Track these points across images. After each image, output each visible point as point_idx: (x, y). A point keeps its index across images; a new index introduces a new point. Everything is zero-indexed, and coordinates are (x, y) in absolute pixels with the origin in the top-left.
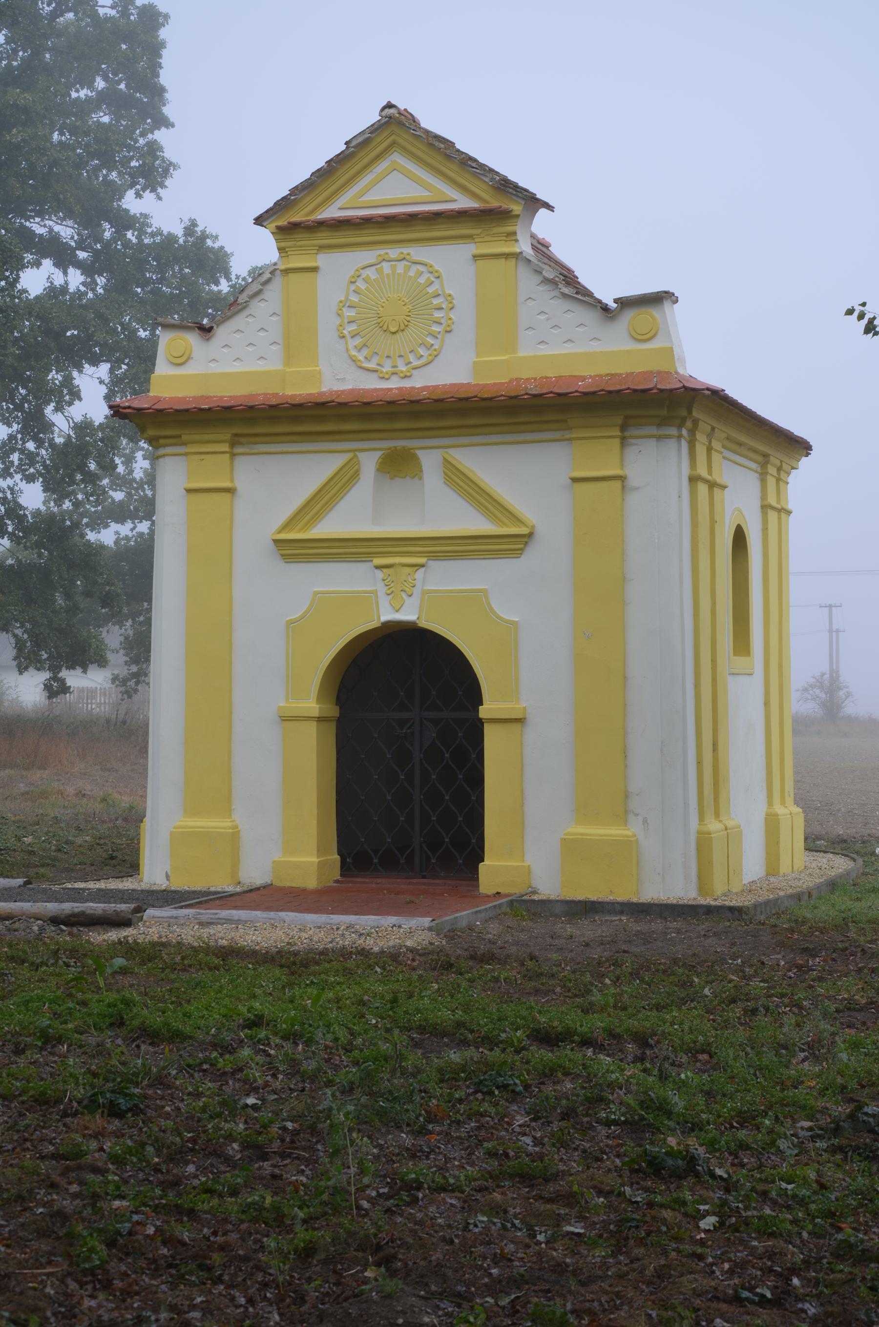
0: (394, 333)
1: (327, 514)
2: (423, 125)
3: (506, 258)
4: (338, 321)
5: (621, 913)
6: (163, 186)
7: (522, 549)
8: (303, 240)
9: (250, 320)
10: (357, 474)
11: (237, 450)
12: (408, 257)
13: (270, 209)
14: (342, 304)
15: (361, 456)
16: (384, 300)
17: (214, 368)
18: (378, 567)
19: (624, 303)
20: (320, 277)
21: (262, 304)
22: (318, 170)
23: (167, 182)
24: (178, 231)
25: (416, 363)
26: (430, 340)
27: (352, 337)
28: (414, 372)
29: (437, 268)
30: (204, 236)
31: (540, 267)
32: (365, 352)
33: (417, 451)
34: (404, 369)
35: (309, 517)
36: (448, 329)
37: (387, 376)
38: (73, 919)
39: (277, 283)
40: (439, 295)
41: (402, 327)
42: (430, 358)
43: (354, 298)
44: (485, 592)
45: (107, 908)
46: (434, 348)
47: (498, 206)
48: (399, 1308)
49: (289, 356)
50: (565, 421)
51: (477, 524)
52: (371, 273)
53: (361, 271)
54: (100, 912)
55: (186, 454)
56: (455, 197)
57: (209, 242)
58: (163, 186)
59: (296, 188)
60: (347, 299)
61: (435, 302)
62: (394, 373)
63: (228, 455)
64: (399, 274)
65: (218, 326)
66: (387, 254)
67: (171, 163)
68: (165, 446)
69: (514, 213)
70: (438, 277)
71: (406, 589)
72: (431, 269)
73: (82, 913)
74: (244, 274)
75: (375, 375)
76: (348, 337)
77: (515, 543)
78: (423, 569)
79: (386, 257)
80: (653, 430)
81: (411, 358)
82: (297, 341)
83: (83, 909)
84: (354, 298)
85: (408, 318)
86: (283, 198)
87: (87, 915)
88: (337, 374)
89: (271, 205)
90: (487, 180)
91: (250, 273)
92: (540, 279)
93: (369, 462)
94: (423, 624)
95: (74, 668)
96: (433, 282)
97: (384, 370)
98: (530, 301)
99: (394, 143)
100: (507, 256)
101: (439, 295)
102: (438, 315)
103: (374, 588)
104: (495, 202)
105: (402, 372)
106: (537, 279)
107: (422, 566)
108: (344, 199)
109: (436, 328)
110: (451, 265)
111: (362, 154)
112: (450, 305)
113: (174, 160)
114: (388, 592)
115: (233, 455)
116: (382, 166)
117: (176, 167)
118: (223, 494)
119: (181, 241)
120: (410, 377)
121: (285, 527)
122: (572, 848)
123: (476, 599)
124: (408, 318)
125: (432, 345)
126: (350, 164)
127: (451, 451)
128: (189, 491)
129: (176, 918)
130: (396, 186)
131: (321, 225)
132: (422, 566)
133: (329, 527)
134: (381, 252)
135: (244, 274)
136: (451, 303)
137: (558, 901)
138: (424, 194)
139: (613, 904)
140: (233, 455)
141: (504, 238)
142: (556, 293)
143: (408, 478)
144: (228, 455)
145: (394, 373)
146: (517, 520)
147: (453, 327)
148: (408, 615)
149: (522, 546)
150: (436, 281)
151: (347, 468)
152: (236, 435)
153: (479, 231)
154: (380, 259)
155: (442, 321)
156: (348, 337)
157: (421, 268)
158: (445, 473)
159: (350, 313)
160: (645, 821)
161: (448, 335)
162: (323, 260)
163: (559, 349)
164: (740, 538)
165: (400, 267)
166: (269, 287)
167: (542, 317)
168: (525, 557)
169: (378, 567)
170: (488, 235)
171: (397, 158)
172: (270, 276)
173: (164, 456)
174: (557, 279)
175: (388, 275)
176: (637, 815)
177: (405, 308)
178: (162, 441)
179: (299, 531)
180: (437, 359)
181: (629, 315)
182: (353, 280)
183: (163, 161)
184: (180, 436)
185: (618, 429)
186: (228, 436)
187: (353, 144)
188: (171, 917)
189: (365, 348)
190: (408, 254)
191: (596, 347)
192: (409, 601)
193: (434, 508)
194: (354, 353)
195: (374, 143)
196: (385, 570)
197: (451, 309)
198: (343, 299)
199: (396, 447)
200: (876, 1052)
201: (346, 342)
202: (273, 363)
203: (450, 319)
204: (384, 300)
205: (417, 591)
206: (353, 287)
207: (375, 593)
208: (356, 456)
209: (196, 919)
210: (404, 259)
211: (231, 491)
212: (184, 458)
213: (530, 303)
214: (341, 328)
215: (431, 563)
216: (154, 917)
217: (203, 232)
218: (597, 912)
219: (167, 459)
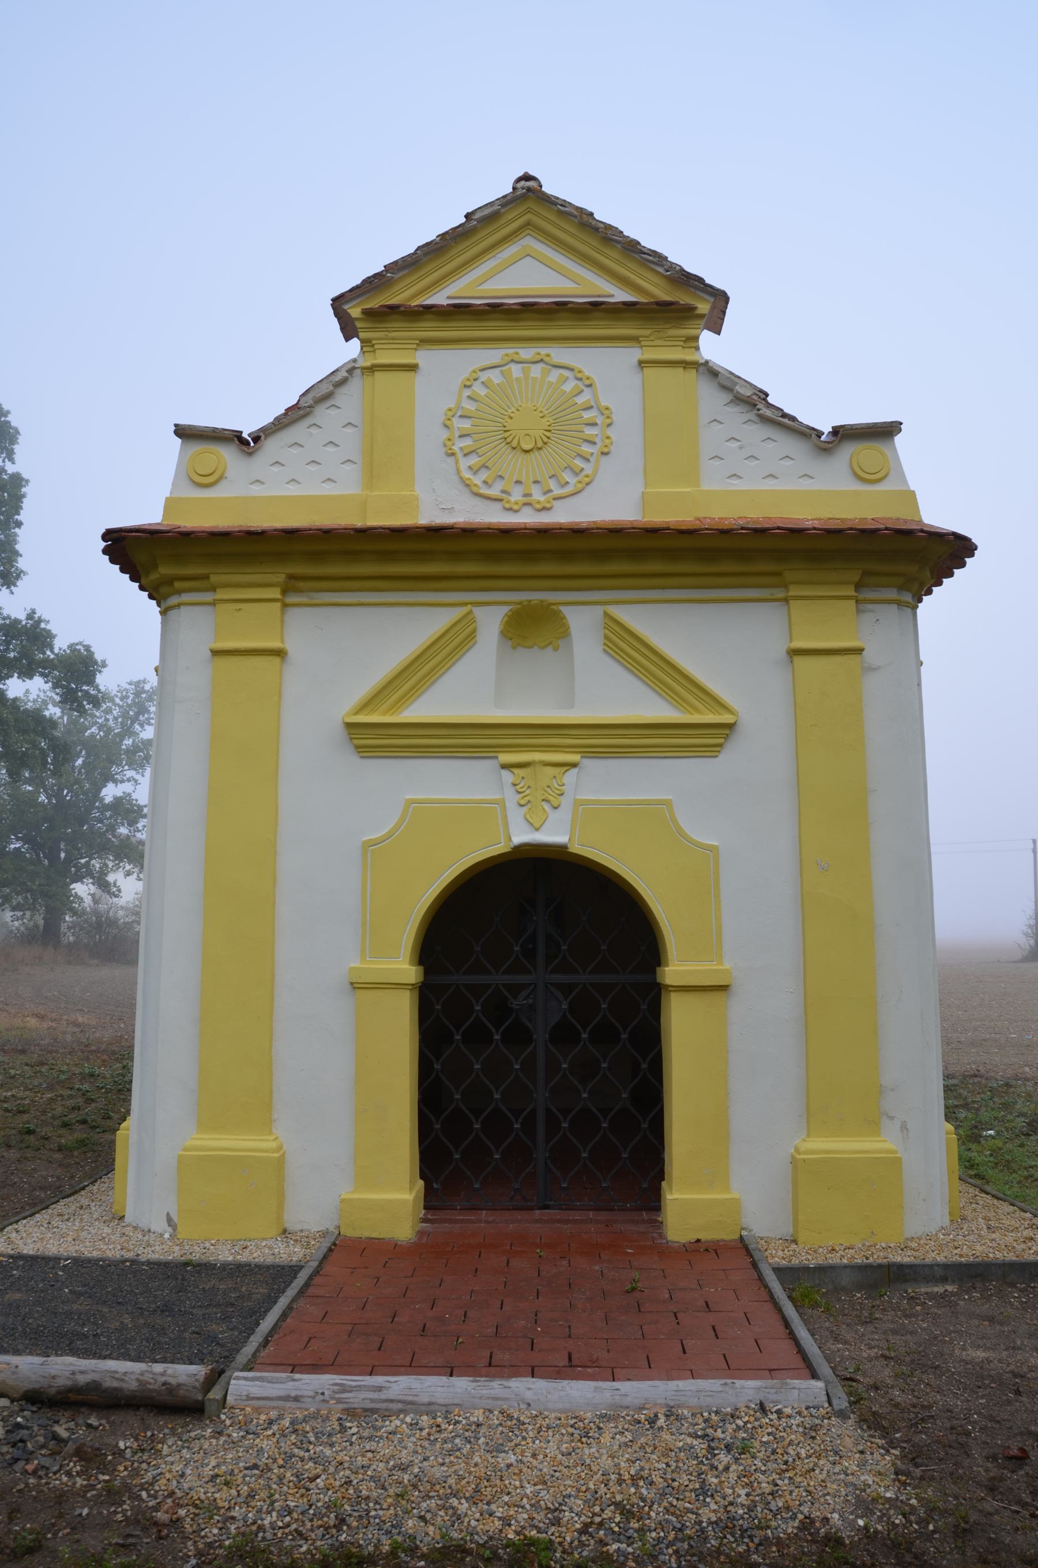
0: (526, 452)
1: (418, 697)
3: (684, 368)
4: (445, 434)
5: (944, 1280)
6: (15, 585)
7: (720, 745)
8: (398, 329)
9: (314, 430)
10: (471, 637)
11: (291, 599)
12: (546, 359)
13: (357, 287)
15: (478, 611)
16: (513, 409)
18: (504, 766)
19: (842, 434)
20: (419, 381)
21: (333, 412)
22: (428, 244)
23: (19, 583)
24: (22, 616)
25: (558, 492)
26: (579, 463)
27: (465, 455)
28: (556, 503)
29: (587, 374)
30: (40, 620)
31: (733, 381)
32: (484, 475)
33: (562, 608)
34: (542, 499)
35: (401, 692)
36: (606, 450)
37: (516, 507)
38: (72, 1397)
39: (356, 384)
40: (592, 407)
41: (540, 444)
42: (580, 486)
43: (470, 406)
44: (667, 803)
45: (147, 1377)
46: (583, 473)
47: (669, 303)
49: (371, 475)
50: (779, 574)
51: (658, 710)
52: (495, 376)
53: (480, 374)
54: (132, 1385)
55: (213, 603)
56: (612, 292)
57: (43, 625)
58: (15, 585)
59: (396, 263)
60: (459, 406)
61: (587, 415)
62: (525, 504)
63: (279, 604)
64: (535, 379)
65: (266, 437)
66: (517, 353)
67: (22, 571)
68: (179, 592)
69: (698, 312)
70: (590, 386)
71: (551, 798)
72: (579, 375)
73: (94, 1387)
74: (65, 647)
75: (498, 506)
76: (460, 455)
78: (575, 771)
79: (516, 358)
80: (892, 594)
81: (552, 484)
83: (96, 1377)
84: (470, 406)
85: (548, 434)
86: (375, 276)
87: (106, 1390)
88: (438, 499)
89: (359, 282)
90: (661, 270)
91: (68, 647)
92: (728, 397)
93: (491, 621)
94: (576, 848)
96: (582, 391)
97: (513, 499)
98: (715, 423)
99: (528, 224)
100: (686, 365)
101: (592, 407)
102: (590, 431)
103: (497, 797)
105: (539, 502)
106: (727, 397)
107: (574, 765)
109: (586, 448)
110: (609, 371)
111: (484, 233)
112: (608, 421)
113: (24, 569)
114: (522, 802)
115: (285, 606)
116: (510, 250)
117: (25, 573)
118: (270, 658)
119: (24, 623)
120: (549, 509)
121: (365, 706)
123: (658, 814)
124: (548, 434)
125: (582, 470)
126: (467, 243)
128: (216, 653)
129: (296, 1399)
131: (429, 310)
132: (574, 765)
133: (427, 708)
135: (65, 647)
136: (608, 417)
137: (846, 1267)
139: (931, 1266)
140: (285, 606)
141: (682, 343)
142: (752, 415)
143: (536, 647)
144: (279, 604)
145: (525, 504)
146: (725, 708)
147: (612, 448)
148: (554, 832)
149: (722, 740)
150: (587, 390)
151: (457, 629)
152: (291, 577)
153: (648, 332)
154: (508, 359)
155: (597, 440)
156: (460, 455)
157: (566, 373)
158: (606, 637)
160: (904, 1127)
161: (604, 458)
162: (422, 357)
163: (746, 485)
165: (536, 371)
166: (343, 389)
167: (734, 445)
168: (721, 756)
169: (504, 766)
170: (660, 338)
171: (529, 242)
172: (346, 374)
173: (179, 605)
174: (755, 397)
175: (518, 379)
176: (892, 1118)
177: (543, 420)
178: (177, 585)
179: (385, 713)
180: (589, 488)
181: (848, 451)
182: (468, 383)
183: (17, 569)
184: (206, 577)
185: (853, 587)
186: (281, 578)
187: (477, 216)
188: (286, 1398)
189: (483, 470)
190: (548, 355)
191: (806, 485)
194: (467, 475)
195: (503, 221)
196: (516, 771)
197: (609, 425)
198: (452, 406)
199: (530, 601)
201: (457, 462)
203: (608, 438)
204: (513, 409)
205: (566, 802)
206: (467, 392)
207: (501, 803)
208: (470, 612)
209: (339, 1401)
210: (542, 360)
211: (279, 653)
212: (209, 609)
213: (716, 427)
214: (449, 443)
215: (586, 762)
216: (249, 1398)
217: (40, 618)
218: (906, 1281)
219: (184, 609)
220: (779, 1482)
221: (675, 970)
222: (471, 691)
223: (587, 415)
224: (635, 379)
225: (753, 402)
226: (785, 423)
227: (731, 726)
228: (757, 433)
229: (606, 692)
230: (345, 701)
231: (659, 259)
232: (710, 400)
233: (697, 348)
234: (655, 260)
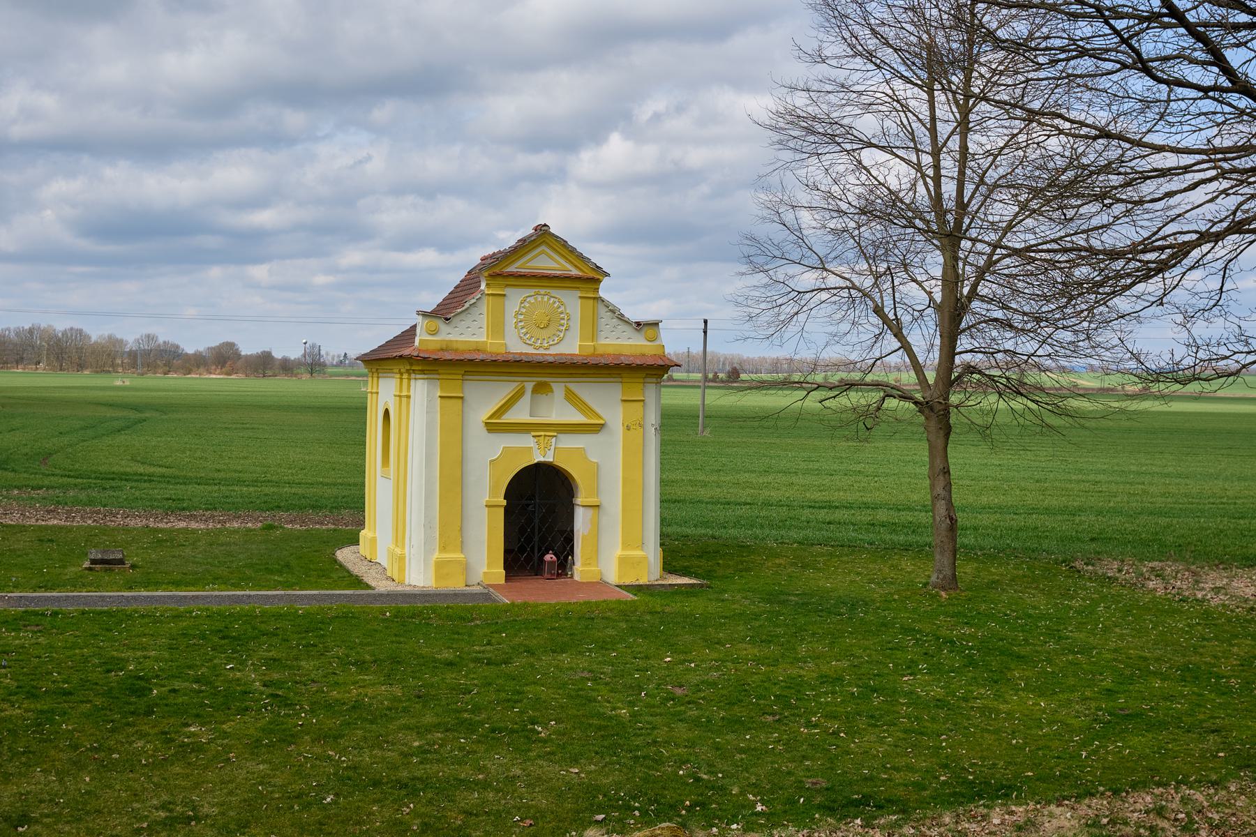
2: (190, 350)
8: (500, 281)
10: (523, 394)
14: (517, 314)
17: (451, 337)
47: (588, 279)
77: (597, 428)
82: (497, 327)
88: (515, 344)
93: (529, 386)
108: (518, 264)
110: (571, 302)
122: (623, 561)
131: (511, 275)
133: (509, 417)
146: (601, 418)
162: (507, 291)
163: (617, 342)
164: (387, 412)
165: (546, 298)
191: (630, 342)
193: (558, 410)
200: (1253, 822)
227: (603, 425)
230: (484, 414)
233: (597, 290)
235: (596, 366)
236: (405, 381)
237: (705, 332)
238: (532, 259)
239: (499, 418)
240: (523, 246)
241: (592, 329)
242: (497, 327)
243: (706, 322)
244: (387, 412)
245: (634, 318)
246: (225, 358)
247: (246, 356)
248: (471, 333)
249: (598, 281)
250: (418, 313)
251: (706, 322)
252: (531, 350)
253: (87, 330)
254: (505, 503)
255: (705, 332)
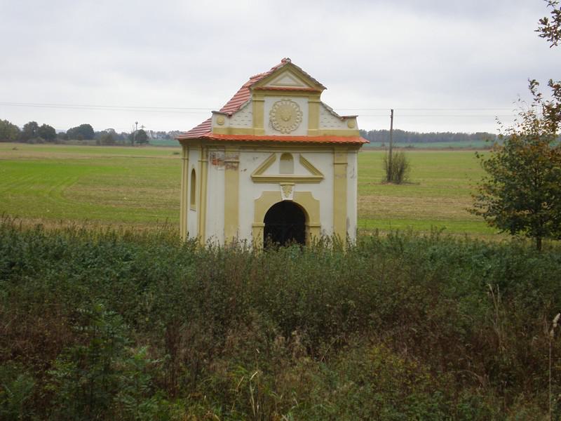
10: (275, 160)
14: (271, 111)
15: (277, 154)
19: (345, 118)
20: (265, 103)
43: (275, 110)
47: (314, 90)
48: (372, 340)
49: (255, 125)
52: (280, 104)
61: (298, 113)
77: (318, 180)
82: (257, 121)
84: (275, 110)
88: (268, 132)
93: (278, 156)
94: (294, 201)
95: (26, 126)
104: (316, 88)
108: (272, 82)
110: (302, 103)
116: (284, 74)
127: (302, 154)
130: (287, 81)
133: (267, 174)
134: (282, 98)
138: (295, 83)
146: (321, 174)
148: (290, 198)
159: (274, 114)
162: (266, 99)
163: (328, 129)
164: (193, 171)
165: (288, 103)
191: (340, 129)
192: (290, 195)
202: (249, 126)
205: (292, 192)
220: (169, 259)
221: (311, 222)
222: (274, 171)
223: (298, 113)
224: (307, 105)
225: (329, 111)
226: (335, 115)
227: (322, 178)
228: (330, 116)
229: (300, 171)
231: (314, 80)
232: (322, 109)
233: (319, 97)
234: (313, 80)
235: (318, 144)
236: (204, 153)
237: (392, 117)
238: (281, 79)
239: (260, 174)
240: (275, 72)
241: (313, 120)
242: (257, 121)
243: (392, 111)
244: (193, 171)
245: (341, 115)
246: (84, 134)
247: (98, 133)
248: (242, 125)
249: (320, 93)
250: (212, 112)
251: (392, 111)
252: (279, 134)
253: (38, 123)
254: (264, 225)
255: (392, 117)
